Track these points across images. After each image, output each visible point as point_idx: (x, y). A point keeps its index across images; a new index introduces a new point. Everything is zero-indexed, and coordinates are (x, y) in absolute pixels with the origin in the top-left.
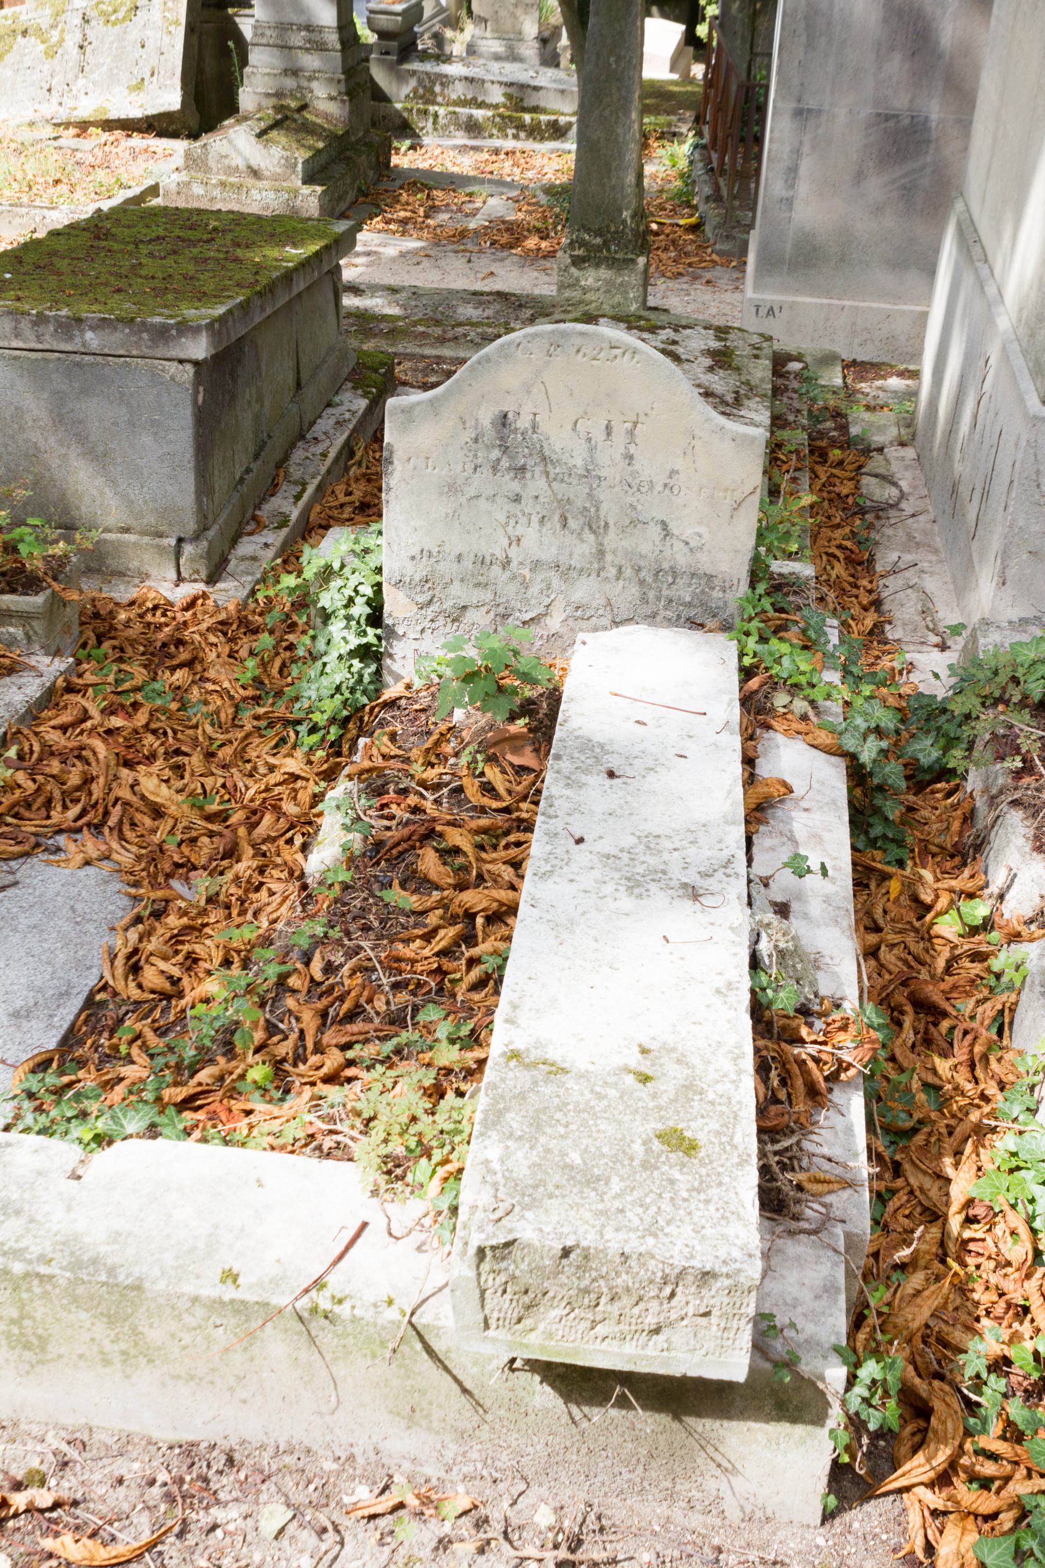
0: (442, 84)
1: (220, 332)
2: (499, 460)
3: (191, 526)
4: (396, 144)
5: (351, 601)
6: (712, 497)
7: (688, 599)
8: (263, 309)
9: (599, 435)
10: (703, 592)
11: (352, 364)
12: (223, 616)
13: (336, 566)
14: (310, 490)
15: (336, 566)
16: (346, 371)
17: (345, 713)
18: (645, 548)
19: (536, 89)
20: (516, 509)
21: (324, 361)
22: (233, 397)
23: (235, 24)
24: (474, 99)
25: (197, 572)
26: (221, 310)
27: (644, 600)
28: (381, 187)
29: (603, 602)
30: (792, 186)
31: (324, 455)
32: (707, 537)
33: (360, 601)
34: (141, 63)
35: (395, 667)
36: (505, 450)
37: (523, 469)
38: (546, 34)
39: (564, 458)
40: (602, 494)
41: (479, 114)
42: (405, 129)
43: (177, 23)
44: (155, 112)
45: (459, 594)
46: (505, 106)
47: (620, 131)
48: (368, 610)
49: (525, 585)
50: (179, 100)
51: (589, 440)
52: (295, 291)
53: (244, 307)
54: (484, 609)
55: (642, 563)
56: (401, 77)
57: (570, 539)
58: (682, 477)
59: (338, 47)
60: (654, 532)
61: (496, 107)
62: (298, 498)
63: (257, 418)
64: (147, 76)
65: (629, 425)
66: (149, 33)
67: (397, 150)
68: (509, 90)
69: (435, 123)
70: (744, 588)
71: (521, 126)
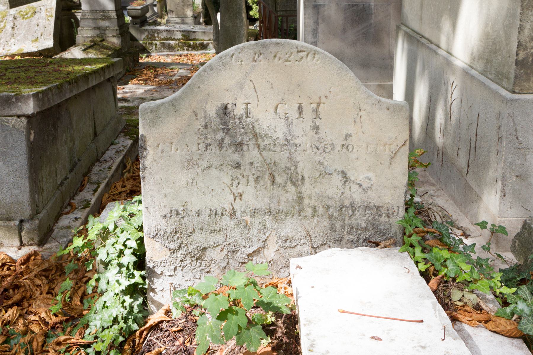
0: (158, 33)
1: (43, 99)
2: (223, 139)
3: (27, 212)
4: (141, 55)
5: (121, 253)
6: (376, 150)
7: (364, 225)
8: (71, 91)
9: (293, 114)
10: (374, 219)
11: (124, 125)
12: (46, 265)
13: (111, 228)
14: (102, 186)
15: (111, 228)
16: (120, 128)
17: (121, 339)
18: (331, 192)
19: (194, 32)
20: (237, 173)
21: (109, 123)
22: (55, 138)
23: (75, 16)
24: (171, 37)
25: (32, 239)
26: (44, 88)
27: (333, 229)
28: (136, 69)
29: (304, 233)
30: (316, 37)
31: (110, 168)
32: (374, 179)
33: (128, 252)
34: (37, 32)
35: (157, 297)
36: (227, 131)
37: (241, 144)
38: (196, 15)
39: (270, 133)
40: (299, 157)
41: (172, 43)
42: (144, 50)
43: (52, 16)
44: (42, 48)
45: (200, 238)
46: (182, 39)
47: (238, 22)
48: (134, 259)
49: (248, 227)
50: (52, 43)
51: (287, 119)
52: (91, 85)
53: (60, 88)
54: (219, 248)
55: (330, 203)
56: (142, 32)
57: (278, 191)
58: (354, 138)
59: (116, 17)
60: (337, 179)
61: (179, 40)
62: (95, 191)
63: (71, 150)
64: (39, 36)
65: (314, 106)
66: (40, 21)
67: (142, 58)
68: (184, 33)
69: (156, 47)
70: (402, 213)
71: (189, 46)
